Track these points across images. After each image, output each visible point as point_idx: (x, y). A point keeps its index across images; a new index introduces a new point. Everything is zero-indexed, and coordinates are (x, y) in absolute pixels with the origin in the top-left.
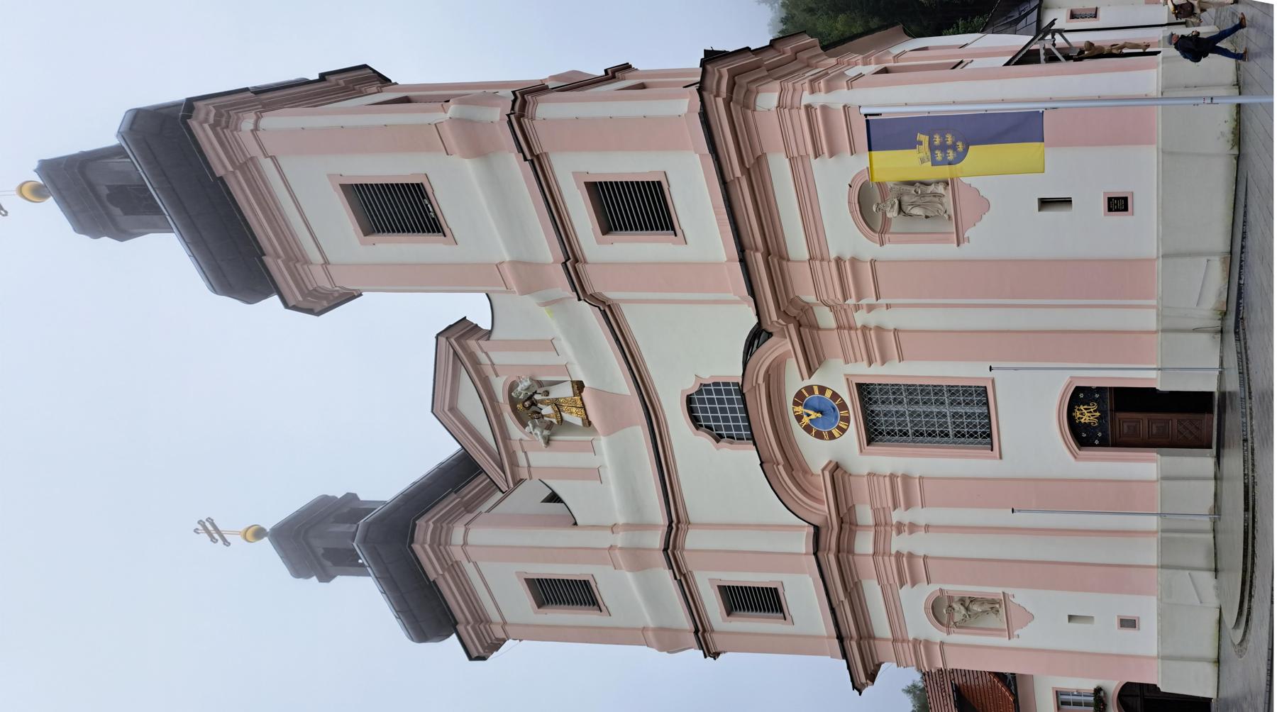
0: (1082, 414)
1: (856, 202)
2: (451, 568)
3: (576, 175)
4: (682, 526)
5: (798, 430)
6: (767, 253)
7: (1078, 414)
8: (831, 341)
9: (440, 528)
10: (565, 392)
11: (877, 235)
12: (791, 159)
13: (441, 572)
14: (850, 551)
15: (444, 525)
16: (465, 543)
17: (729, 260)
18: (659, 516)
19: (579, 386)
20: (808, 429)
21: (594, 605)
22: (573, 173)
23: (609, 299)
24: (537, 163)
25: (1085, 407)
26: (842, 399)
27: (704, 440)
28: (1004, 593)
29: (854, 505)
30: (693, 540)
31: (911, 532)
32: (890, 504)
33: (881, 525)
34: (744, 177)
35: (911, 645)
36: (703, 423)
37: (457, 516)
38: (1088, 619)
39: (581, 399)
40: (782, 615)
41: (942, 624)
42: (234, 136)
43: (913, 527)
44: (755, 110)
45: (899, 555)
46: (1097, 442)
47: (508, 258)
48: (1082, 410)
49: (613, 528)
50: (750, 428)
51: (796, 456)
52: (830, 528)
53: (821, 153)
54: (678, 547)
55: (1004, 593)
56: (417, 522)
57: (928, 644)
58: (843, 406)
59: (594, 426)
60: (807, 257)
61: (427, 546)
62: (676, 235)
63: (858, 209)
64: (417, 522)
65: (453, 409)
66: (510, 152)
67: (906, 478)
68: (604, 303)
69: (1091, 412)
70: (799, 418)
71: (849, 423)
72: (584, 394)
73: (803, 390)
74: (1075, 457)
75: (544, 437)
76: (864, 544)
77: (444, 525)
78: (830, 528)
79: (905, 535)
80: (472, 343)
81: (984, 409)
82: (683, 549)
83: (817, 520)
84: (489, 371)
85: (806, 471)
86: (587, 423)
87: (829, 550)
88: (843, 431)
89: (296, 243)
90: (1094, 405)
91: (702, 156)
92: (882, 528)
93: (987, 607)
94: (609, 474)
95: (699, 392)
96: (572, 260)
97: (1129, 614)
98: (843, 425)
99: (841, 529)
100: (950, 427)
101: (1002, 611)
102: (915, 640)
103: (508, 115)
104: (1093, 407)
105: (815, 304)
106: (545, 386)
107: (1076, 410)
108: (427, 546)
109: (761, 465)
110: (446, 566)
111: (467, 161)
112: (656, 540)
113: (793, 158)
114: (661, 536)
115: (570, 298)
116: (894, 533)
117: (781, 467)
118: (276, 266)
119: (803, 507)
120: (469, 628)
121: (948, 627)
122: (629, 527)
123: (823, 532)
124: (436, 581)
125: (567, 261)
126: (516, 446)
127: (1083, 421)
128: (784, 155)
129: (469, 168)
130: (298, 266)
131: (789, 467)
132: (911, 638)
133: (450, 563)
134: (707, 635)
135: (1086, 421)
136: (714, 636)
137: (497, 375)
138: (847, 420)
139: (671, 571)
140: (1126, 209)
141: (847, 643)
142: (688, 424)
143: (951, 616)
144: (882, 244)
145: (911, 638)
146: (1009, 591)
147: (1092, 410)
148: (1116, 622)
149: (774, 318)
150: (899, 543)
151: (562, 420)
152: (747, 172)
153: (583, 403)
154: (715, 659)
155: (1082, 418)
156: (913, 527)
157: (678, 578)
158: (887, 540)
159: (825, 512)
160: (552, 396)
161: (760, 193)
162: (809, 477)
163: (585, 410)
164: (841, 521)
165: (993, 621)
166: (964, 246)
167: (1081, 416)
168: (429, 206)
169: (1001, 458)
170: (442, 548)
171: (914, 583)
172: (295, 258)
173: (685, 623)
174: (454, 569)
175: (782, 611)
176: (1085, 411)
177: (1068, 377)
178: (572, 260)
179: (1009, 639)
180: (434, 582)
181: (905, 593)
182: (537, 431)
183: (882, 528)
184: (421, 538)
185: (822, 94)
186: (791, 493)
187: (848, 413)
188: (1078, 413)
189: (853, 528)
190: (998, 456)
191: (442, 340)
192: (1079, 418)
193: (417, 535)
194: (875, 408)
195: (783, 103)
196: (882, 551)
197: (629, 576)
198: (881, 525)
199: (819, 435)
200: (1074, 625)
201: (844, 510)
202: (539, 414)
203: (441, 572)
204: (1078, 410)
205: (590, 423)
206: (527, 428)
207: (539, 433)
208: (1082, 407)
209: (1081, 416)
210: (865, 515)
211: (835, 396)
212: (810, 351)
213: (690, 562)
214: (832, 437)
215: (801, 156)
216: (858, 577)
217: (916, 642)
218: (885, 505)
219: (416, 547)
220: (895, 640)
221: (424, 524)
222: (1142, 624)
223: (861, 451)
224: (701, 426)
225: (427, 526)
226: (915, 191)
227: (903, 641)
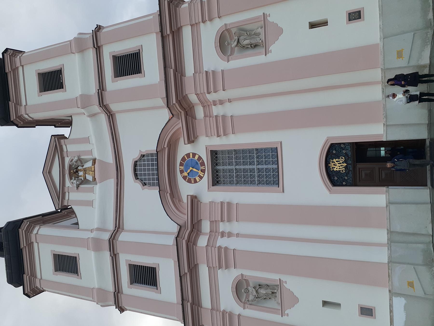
0: (334, 165)
1: (235, 288)
2: (29, 245)
3: (126, 261)
4: (120, 230)
5: (179, 177)
6: (176, 71)
7: (332, 165)
8: (200, 127)
9: (31, 225)
10: (89, 165)
11: (226, 57)
12: (209, 268)
13: (10, 70)
14: (195, 243)
15: (33, 225)
16: (37, 233)
17: (177, 303)
18: (111, 226)
19: (94, 161)
20: (185, 178)
21: (76, 273)
22: (125, 260)
23: (112, 111)
24: (114, 257)
25: (337, 160)
26: (203, 160)
27: (138, 185)
28: (280, 279)
29: (201, 220)
30: (123, 237)
31: (229, 237)
32: (217, 265)
33: (214, 232)
34: (189, 273)
35: (221, 313)
36: (139, 177)
37: (38, 224)
38: (337, 305)
39: (94, 167)
40: (156, 287)
41: (241, 301)
42: (15, 59)
43: (230, 235)
44: (185, 76)
45: (220, 248)
46: (344, 183)
47: (97, 286)
48: (335, 162)
49: (92, 231)
50: (158, 179)
51: (177, 192)
52: (187, 229)
53: (222, 267)
54: (115, 239)
55: (280, 279)
56: (24, 220)
57: (231, 315)
58: (203, 164)
59: (96, 181)
60: (210, 308)
61: (24, 231)
62: (157, 289)
63: (235, 291)
64: (24, 220)
65: (50, 172)
66: (108, 251)
67: (229, 204)
68: (110, 112)
69: (340, 163)
70: (182, 172)
71: (204, 173)
72: (96, 165)
73: (185, 156)
74: (330, 191)
75: (77, 185)
76: (202, 242)
77: (33, 225)
78: (187, 229)
79: (225, 238)
80: (62, 141)
81: (275, 166)
82: (117, 240)
83: (180, 223)
84: (65, 155)
85: (180, 200)
86: (94, 179)
87: (184, 239)
88: (201, 178)
89: (20, 94)
90: (342, 158)
91: (174, 261)
92: (214, 233)
93: (269, 291)
94: (96, 204)
95: (140, 159)
96: (117, 292)
97: (368, 303)
98: (201, 174)
99: (192, 231)
100: (256, 172)
101: (278, 294)
102: (224, 311)
103: (98, 90)
104: (342, 160)
105: (197, 104)
106: (81, 161)
107: (331, 162)
108: (24, 231)
109: (159, 191)
110: (28, 243)
111: (92, 252)
112: (106, 236)
113: (210, 267)
114: (109, 235)
115: (98, 113)
116: (219, 237)
117: (168, 195)
118: (26, 278)
119: (175, 215)
120: (28, 277)
121: (244, 303)
122: (98, 229)
123: (183, 229)
124: (8, 73)
125: (115, 292)
126: (66, 190)
127: (335, 169)
128: (206, 266)
129: (92, 254)
130: (18, 106)
131: (172, 195)
132: (222, 310)
133: (30, 242)
134: (119, 295)
135: (337, 170)
136: (122, 295)
137: (67, 157)
138: (203, 171)
139: (110, 252)
140: (360, 18)
141: (185, 303)
142: (133, 178)
143: (247, 297)
144: (228, 61)
145: (222, 310)
146: (284, 278)
147: (341, 162)
148: (357, 311)
149: (174, 102)
150: (221, 242)
151: (85, 178)
152: (172, 32)
153: (94, 169)
154: (121, 313)
155: (335, 167)
156: (230, 235)
157: (112, 256)
158: (215, 239)
159: (186, 219)
160: (84, 167)
161: (176, 40)
162: (181, 203)
163: (95, 172)
164: (193, 226)
165: (273, 304)
166: (285, 317)
167: (334, 166)
168: (61, 78)
169: (283, 192)
170: (29, 234)
171: (211, 20)
172: (33, 275)
173: (111, 288)
174: (30, 245)
175: (156, 286)
176: (337, 163)
177: (326, 137)
178: (117, 292)
179: (282, 316)
180: (7, 73)
181: (221, 274)
182: (75, 182)
183: (214, 233)
184: (23, 228)
185: (226, 238)
186: (169, 205)
187: (205, 167)
188: (332, 164)
189: (199, 233)
190: (282, 190)
191: (53, 137)
192: (333, 168)
193: (21, 227)
194: (218, 167)
195: (213, 308)
196: (211, 245)
197: (93, 253)
198: (206, 105)
199: (189, 181)
200: (327, 309)
201: (195, 221)
202: (78, 177)
203: (10, 70)
204: (332, 162)
205: (95, 179)
206: (72, 180)
207: (75, 182)
208: (334, 160)
209: (334, 166)
210: (206, 226)
211: (200, 158)
212: (191, 136)
213: (119, 248)
214: (196, 182)
215: (213, 267)
216: (197, 262)
217: (224, 312)
218: (214, 266)
219: (20, 230)
220: (212, 309)
221: (26, 222)
222: (378, 313)
223: (209, 189)
224: (138, 178)
225: (27, 223)
226: (246, 33)
227: (217, 310)
